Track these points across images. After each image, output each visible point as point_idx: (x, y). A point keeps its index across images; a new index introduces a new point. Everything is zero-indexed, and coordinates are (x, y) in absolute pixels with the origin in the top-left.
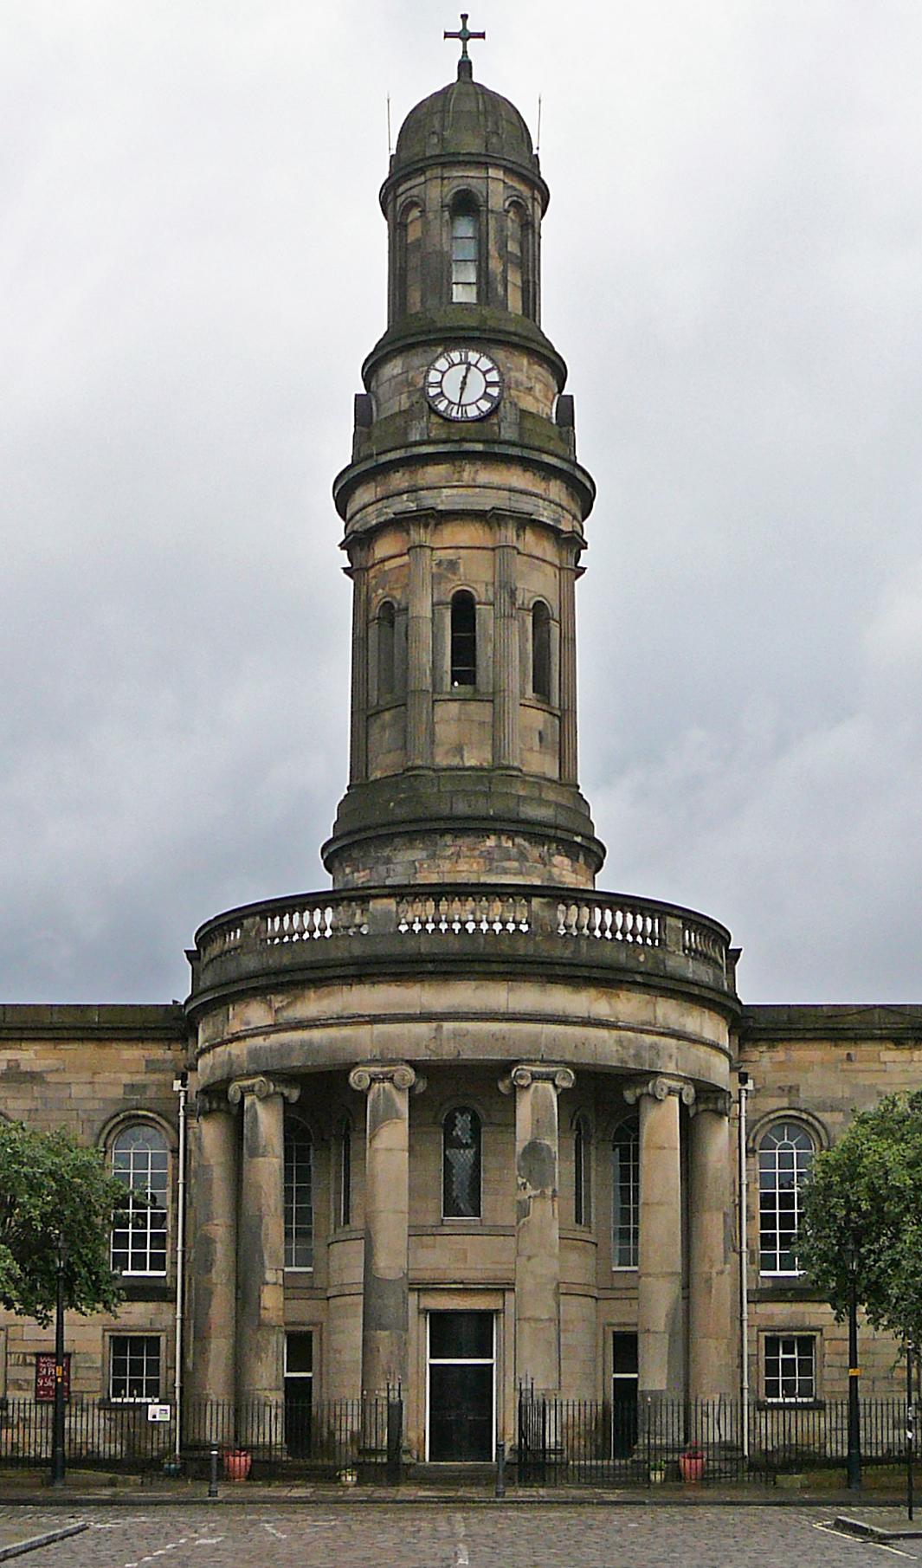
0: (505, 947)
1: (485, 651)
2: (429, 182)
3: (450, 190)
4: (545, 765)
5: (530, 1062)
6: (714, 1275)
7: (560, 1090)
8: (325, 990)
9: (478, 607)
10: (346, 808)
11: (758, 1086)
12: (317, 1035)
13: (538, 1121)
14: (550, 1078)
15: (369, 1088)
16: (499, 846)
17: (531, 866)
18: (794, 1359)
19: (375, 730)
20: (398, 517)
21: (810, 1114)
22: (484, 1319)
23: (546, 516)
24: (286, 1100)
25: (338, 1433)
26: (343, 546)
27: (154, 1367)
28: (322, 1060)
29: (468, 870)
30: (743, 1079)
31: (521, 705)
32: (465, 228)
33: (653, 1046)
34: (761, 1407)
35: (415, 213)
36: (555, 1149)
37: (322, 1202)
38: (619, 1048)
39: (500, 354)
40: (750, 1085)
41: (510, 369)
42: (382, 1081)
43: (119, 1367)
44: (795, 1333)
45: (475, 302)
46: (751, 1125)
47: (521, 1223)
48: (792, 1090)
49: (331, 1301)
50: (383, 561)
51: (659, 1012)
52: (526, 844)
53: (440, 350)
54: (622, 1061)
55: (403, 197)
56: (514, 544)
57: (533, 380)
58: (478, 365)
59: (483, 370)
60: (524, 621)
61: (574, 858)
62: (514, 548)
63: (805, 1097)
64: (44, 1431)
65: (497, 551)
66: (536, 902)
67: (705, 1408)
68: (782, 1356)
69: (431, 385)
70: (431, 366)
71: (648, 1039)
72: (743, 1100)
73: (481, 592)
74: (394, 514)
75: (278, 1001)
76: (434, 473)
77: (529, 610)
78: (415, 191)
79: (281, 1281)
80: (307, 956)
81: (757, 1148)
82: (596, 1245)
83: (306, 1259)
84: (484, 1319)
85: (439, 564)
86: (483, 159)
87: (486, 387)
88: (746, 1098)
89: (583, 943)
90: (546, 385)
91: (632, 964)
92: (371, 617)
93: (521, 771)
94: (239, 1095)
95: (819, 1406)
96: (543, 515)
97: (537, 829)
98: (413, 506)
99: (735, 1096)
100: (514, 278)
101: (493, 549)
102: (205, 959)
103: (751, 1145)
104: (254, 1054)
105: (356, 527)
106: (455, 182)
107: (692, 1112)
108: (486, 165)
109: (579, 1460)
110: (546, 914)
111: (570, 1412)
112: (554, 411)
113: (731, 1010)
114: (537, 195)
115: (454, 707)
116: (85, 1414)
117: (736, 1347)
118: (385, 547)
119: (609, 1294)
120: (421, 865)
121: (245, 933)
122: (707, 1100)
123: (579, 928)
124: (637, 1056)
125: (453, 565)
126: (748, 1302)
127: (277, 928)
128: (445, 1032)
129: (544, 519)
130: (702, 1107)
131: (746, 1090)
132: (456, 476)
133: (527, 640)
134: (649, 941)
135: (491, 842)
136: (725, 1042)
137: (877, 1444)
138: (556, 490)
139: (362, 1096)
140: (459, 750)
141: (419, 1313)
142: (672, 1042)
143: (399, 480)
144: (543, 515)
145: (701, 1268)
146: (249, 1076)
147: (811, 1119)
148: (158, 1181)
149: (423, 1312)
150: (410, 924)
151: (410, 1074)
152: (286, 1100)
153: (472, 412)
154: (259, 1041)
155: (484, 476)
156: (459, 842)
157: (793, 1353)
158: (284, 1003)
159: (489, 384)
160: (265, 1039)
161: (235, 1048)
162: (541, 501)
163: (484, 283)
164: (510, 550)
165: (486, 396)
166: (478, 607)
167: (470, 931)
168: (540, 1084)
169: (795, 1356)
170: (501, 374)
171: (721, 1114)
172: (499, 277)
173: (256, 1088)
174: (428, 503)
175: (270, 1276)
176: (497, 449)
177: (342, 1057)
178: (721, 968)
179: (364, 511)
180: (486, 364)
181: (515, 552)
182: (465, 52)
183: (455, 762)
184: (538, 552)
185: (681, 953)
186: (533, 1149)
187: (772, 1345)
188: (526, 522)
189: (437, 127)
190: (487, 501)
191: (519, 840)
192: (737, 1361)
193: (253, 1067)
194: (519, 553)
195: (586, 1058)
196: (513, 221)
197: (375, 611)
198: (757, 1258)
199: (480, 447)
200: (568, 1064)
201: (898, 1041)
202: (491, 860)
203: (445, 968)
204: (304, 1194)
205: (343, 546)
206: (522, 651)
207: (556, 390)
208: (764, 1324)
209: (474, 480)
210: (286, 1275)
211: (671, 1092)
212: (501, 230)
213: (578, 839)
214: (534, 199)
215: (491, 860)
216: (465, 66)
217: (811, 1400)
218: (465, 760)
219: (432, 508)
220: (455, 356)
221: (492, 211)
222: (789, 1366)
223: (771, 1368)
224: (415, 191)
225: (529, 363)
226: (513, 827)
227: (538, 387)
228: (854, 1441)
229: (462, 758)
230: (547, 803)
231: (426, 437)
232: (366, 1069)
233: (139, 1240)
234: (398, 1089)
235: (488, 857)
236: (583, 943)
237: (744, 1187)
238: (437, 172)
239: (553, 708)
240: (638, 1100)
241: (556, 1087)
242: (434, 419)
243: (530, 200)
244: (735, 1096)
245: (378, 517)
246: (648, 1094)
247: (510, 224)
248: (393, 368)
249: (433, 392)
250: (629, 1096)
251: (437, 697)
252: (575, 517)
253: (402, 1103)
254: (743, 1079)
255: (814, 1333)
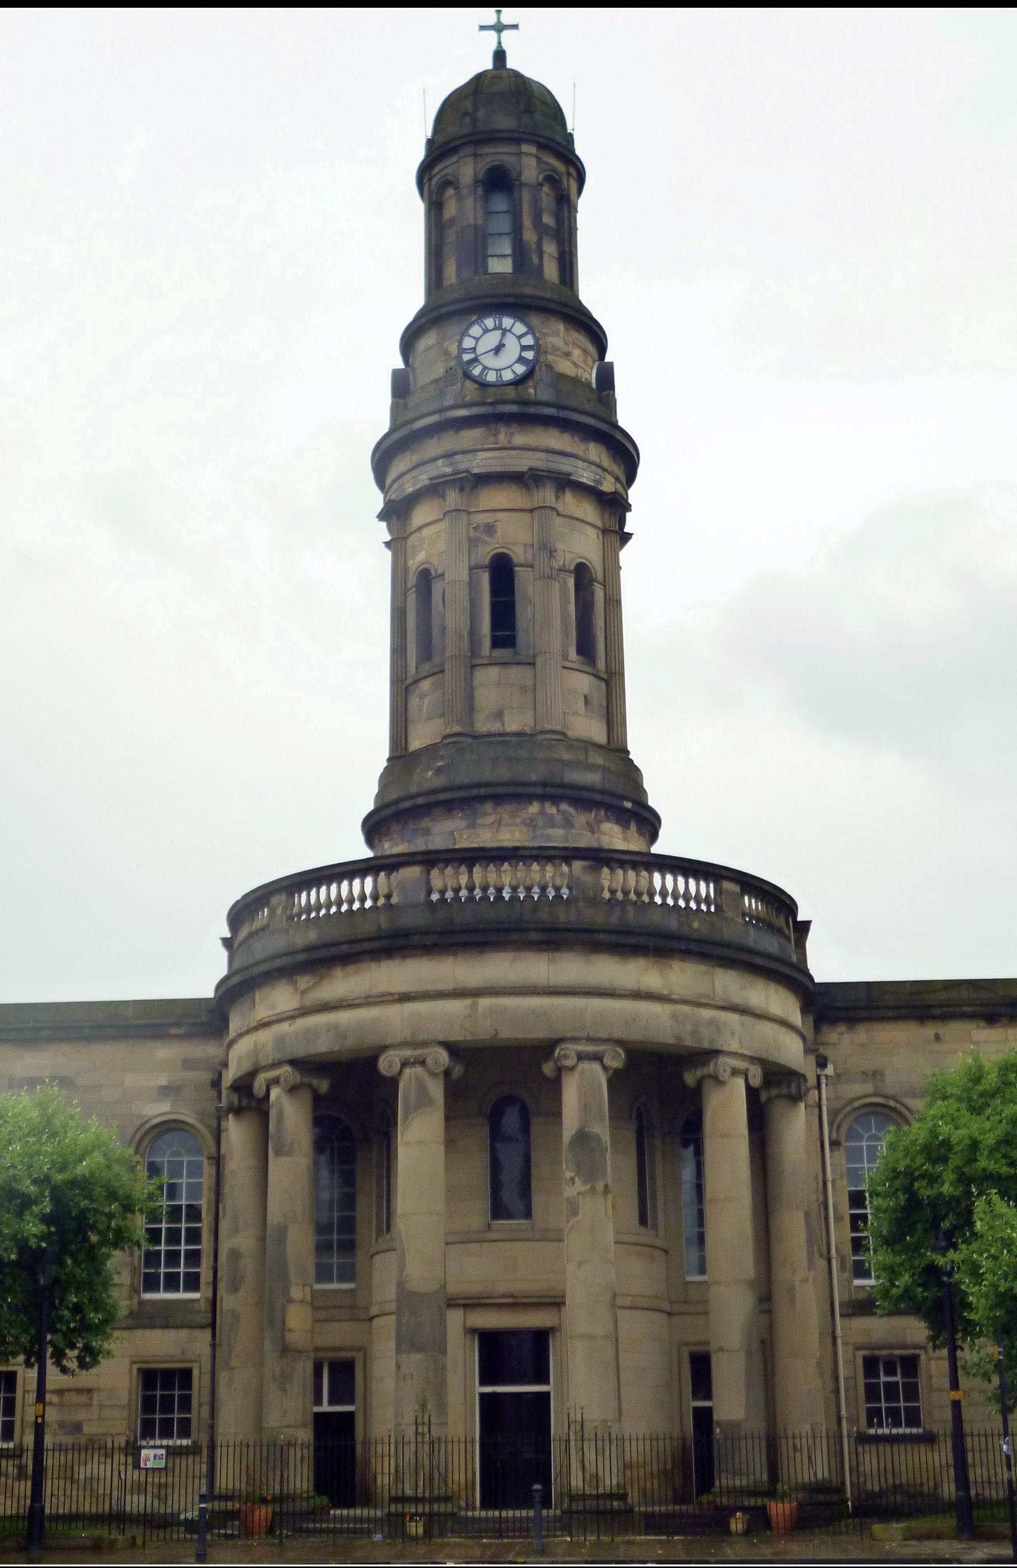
0: (544, 915)
1: (524, 614)
2: (461, 161)
3: (484, 164)
4: (597, 732)
5: (575, 1040)
6: (797, 1284)
7: (611, 1072)
8: (352, 968)
9: (517, 569)
10: (387, 779)
11: (838, 1071)
12: (344, 1017)
13: (585, 1106)
14: (598, 1058)
15: (401, 1071)
16: (542, 812)
17: (579, 834)
18: (897, 1383)
19: (414, 702)
20: (434, 482)
21: (897, 1101)
22: (541, 1339)
23: (586, 476)
24: (315, 1092)
25: (379, 1477)
26: (382, 516)
27: (186, 1403)
28: (350, 1043)
29: (511, 836)
30: (822, 1063)
31: (564, 667)
32: (500, 203)
33: (712, 1022)
34: (863, 1439)
35: (450, 192)
36: (606, 1138)
37: (365, 1209)
38: (674, 1024)
39: (536, 320)
40: (830, 1070)
41: (546, 335)
42: (413, 1064)
43: (148, 1404)
44: (896, 1352)
45: (511, 272)
46: (834, 1114)
47: (570, 1224)
48: (875, 1075)
49: (375, 1321)
50: (420, 528)
51: (718, 985)
52: (571, 810)
53: (474, 318)
54: (679, 1038)
55: (439, 176)
56: (553, 505)
57: (571, 344)
58: (513, 331)
59: (518, 334)
60: (565, 582)
61: (625, 825)
62: (553, 509)
63: (891, 1083)
64: (62, 1482)
65: (536, 514)
66: (578, 865)
67: (798, 1442)
68: (883, 1379)
69: (465, 351)
70: (464, 333)
71: (707, 1014)
72: (823, 1086)
73: (518, 554)
74: (431, 479)
75: (304, 981)
76: (470, 437)
77: (571, 572)
78: (449, 170)
79: (309, 1298)
80: (334, 933)
81: (843, 1139)
82: (666, 1252)
83: (348, 1274)
84: (541, 1339)
85: (476, 529)
86: (516, 135)
87: (521, 352)
88: (826, 1085)
89: (631, 911)
90: (585, 351)
91: (685, 931)
92: (409, 585)
93: (564, 734)
94: (264, 1087)
95: (930, 1439)
96: (583, 476)
97: (587, 795)
98: (448, 470)
99: (812, 1081)
100: (550, 248)
101: (531, 511)
102: (236, 945)
103: (834, 1136)
104: (280, 1042)
105: (393, 497)
106: (490, 159)
107: (764, 1096)
108: (518, 141)
109: (653, 1505)
110: (588, 879)
111: (641, 1449)
112: (594, 376)
113: (806, 988)
114: (572, 171)
115: (494, 672)
116: (109, 1461)
117: (828, 1367)
118: (421, 515)
119: (683, 1308)
120: (461, 835)
121: (272, 912)
122: (779, 1084)
123: (626, 893)
124: (695, 1033)
125: (490, 529)
126: (842, 1316)
127: (303, 902)
128: (480, 1009)
129: (584, 480)
130: (774, 1092)
131: (826, 1076)
132: (491, 439)
133: (569, 602)
134: (704, 907)
135: (534, 808)
136: (796, 1018)
137: (983, 1483)
138: (595, 452)
139: (393, 1083)
140: (499, 715)
141: (465, 1333)
142: (733, 1018)
143: (433, 447)
144: (583, 476)
145: (782, 1275)
146: (275, 1065)
147: (898, 1106)
148: (195, 1190)
149: (472, 1331)
150: (442, 892)
151: (443, 1057)
152: (315, 1092)
153: (508, 376)
154: (285, 1027)
155: (520, 438)
156: (501, 809)
157: (895, 1374)
158: (311, 983)
159: (524, 348)
160: (290, 1025)
161: (264, 1036)
162: (580, 463)
163: (520, 254)
164: (548, 512)
165: (521, 360)
166: (517, 569)
167: (507, 898)
168: (586, 1066)
169: (898, 1378)
170: (536, 339)
171: (795, 1099)
172: (534, 246)
173: (282, 1080)
174: (463, 466)
175: (296, 1293)
176: (532, 410)
177: (372, 1040)
178: (788, 939)
179: (400, 481)
180: (520, 328)
181: (555, 513)
182: (499, 43)
183: (495, 727)
184: (579, 513)
185: (740, 921)
186: (582, 1138)
187: (871, 1365)
188: (565, 483)
189: (470, 108)
190: (522, 463)
191: (564, 807)
192: (830, 1385)
193: (280, 1056)
194: (558, 514)
195: (635, 1035)
196: (548, 194)
197: (412, 580)
198: (849, 1265)
199: (513, 408)
200: (619, 1042)
201: (991, 1019)
202: (535, 827)
203: (480, 938)
204: (348, 1202)
205: (382, 516)
206: (564, 613)
207: (596, 357)
208: (858, 1340)
209: (509, 442)
210: (314, 1293)
211: (735, 1072)
212: (535, 202)
213: (628, 805)
214: (569, 174)
215: (535, 827)
216: (500, 56)
217: (921, 1430)
218: (506, 724)
219: (467, 471)
220: (489, 322)
221: (525, 185)
222: (891, 1390)
223: (871, 1392)
224: (449, 170)
225: (566, 330)
226: (559, 791)
227: (576, 353)
228: (962, 1481)
229: (503, 725)
230: (593, 768)
231: (460, 402)
232: (397, 1053)
233: (173, 1257)
234: (433, 1074)
235: (531, 824)
236: (630, 909)
237: (829, 1185)
238: (470, 150)
239: (599, 671)
240: (700, 1083)
241: (605, 1068)
242: (468, 384)
243: (565, 175)
244: (812, 1081)
245: (414, 484)
246: (710, 1076)
247: (544, 197)
248: (428, 340)
249: (466, 357)
250: (690, 1078)
251: (475, 662)
252: (617, 479)
253: (436, 1090)
254: (822, 1063)
255: (917, 1352)
